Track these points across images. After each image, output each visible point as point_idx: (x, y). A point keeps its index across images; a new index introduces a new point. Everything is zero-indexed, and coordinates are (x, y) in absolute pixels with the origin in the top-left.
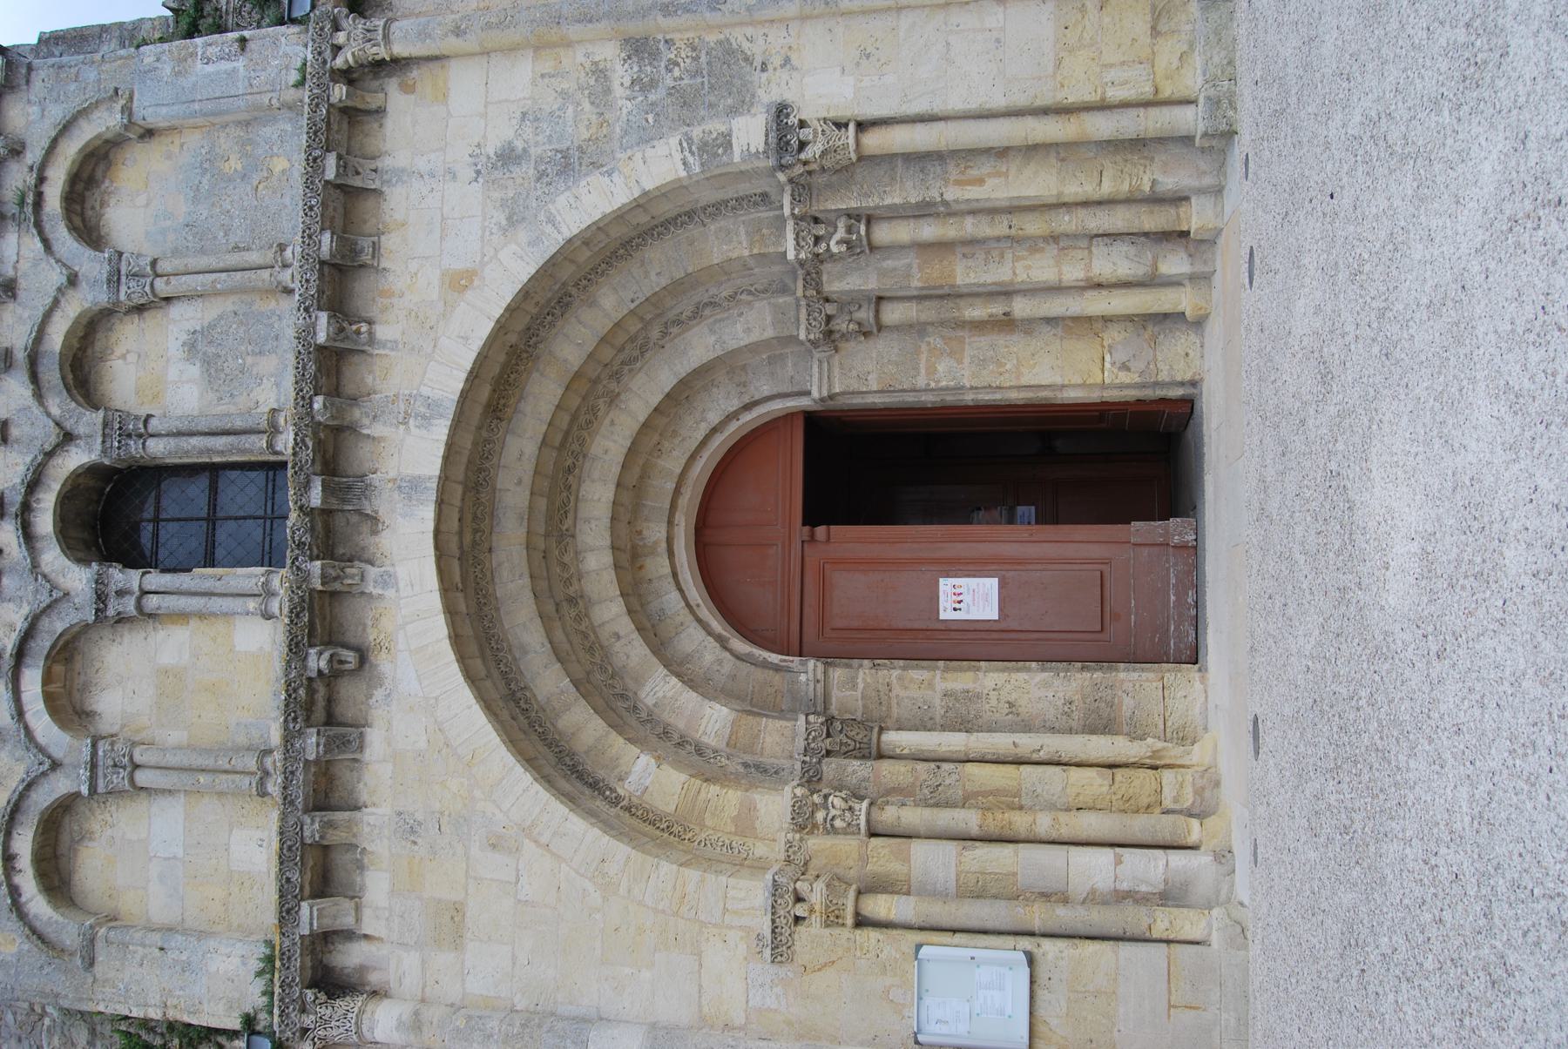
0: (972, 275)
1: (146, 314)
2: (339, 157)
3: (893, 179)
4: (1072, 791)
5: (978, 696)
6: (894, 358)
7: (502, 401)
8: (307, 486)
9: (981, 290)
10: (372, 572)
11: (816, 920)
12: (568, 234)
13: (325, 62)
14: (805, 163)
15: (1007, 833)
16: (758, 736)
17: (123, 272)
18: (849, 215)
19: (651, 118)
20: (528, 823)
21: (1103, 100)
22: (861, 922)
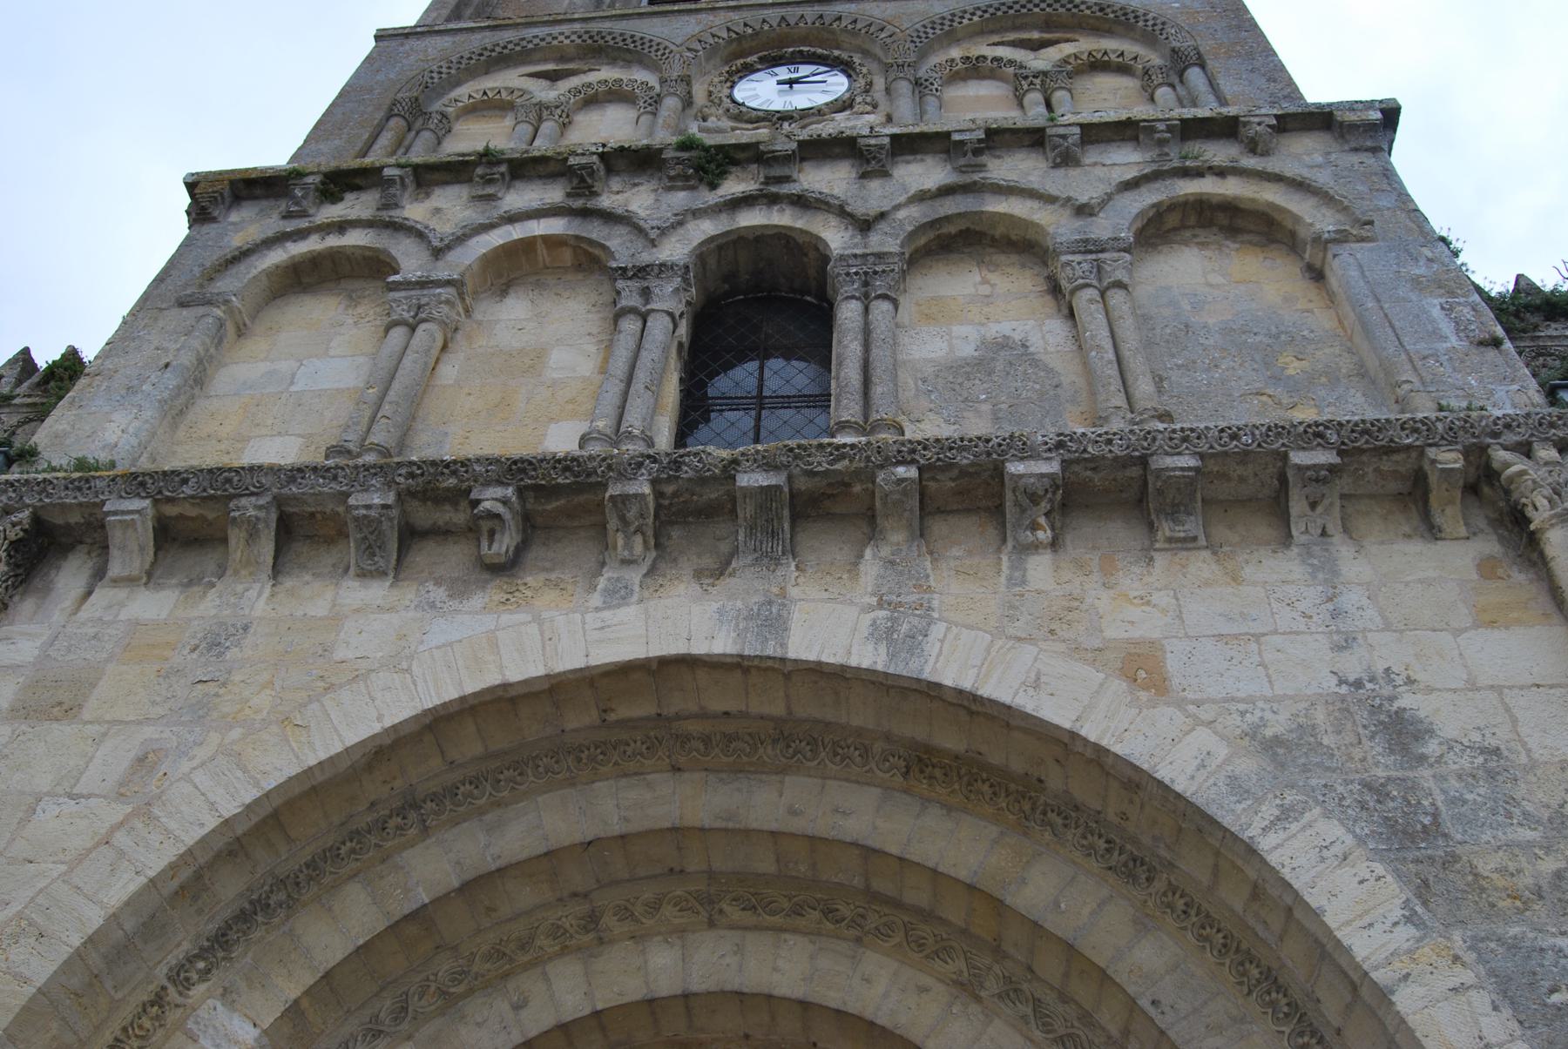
1: (1049, 297)
2: (1332, 469)
7: (938, 773)
8: (769, 465)
12: (1265, 844)
13: (1495, 435)
17: (1101, 256)
20: (156, 811)
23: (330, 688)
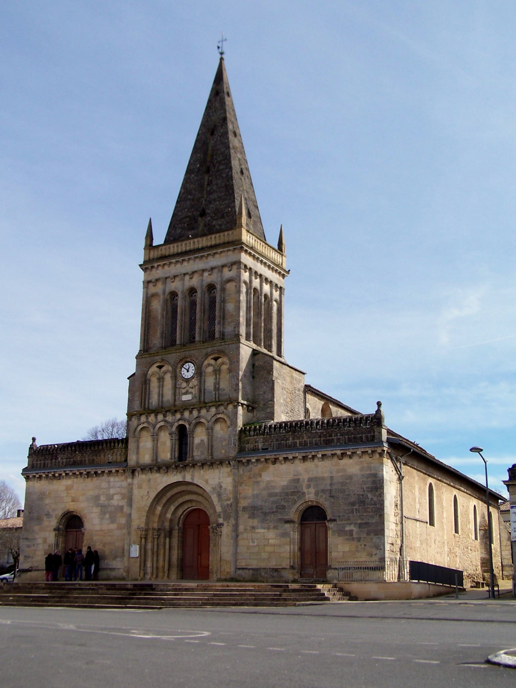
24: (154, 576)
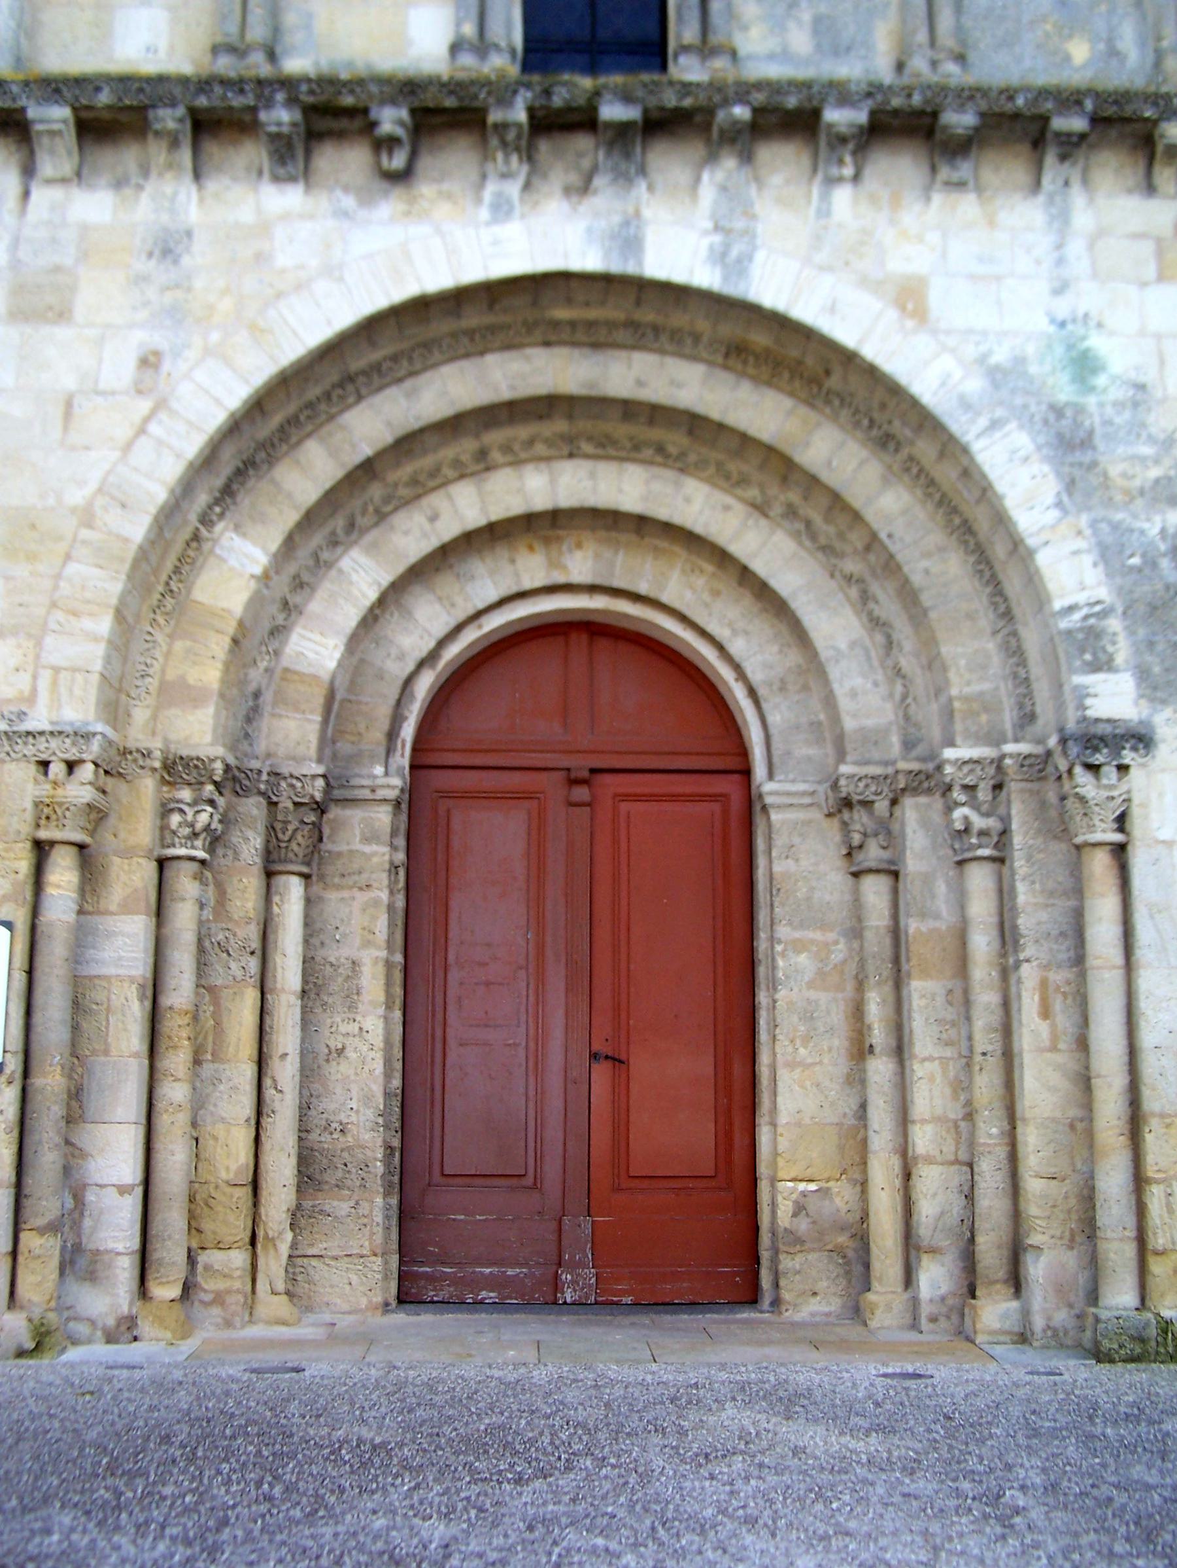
0: (923, 1002)
3: (1051, 894)
4: (220, 1130)
5: (352, 1007)
6: (817, 895)
8: (627, 98)
9: (905, 1013)
10: (513, 189)
11: (44, 790)
14: (1070, 772)
15: (162, 1045)
16: (297, 709)
18: (1005, 832)
19: (1135, 561)
21: (1148, 1181)
22: (41, 849)
23: (279, 295)
24: (165, 1291)
